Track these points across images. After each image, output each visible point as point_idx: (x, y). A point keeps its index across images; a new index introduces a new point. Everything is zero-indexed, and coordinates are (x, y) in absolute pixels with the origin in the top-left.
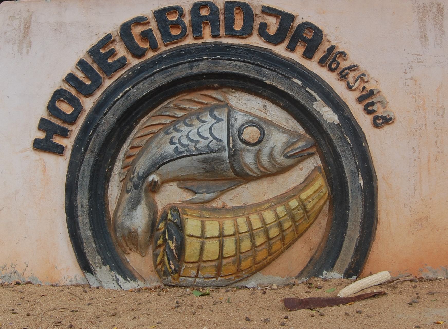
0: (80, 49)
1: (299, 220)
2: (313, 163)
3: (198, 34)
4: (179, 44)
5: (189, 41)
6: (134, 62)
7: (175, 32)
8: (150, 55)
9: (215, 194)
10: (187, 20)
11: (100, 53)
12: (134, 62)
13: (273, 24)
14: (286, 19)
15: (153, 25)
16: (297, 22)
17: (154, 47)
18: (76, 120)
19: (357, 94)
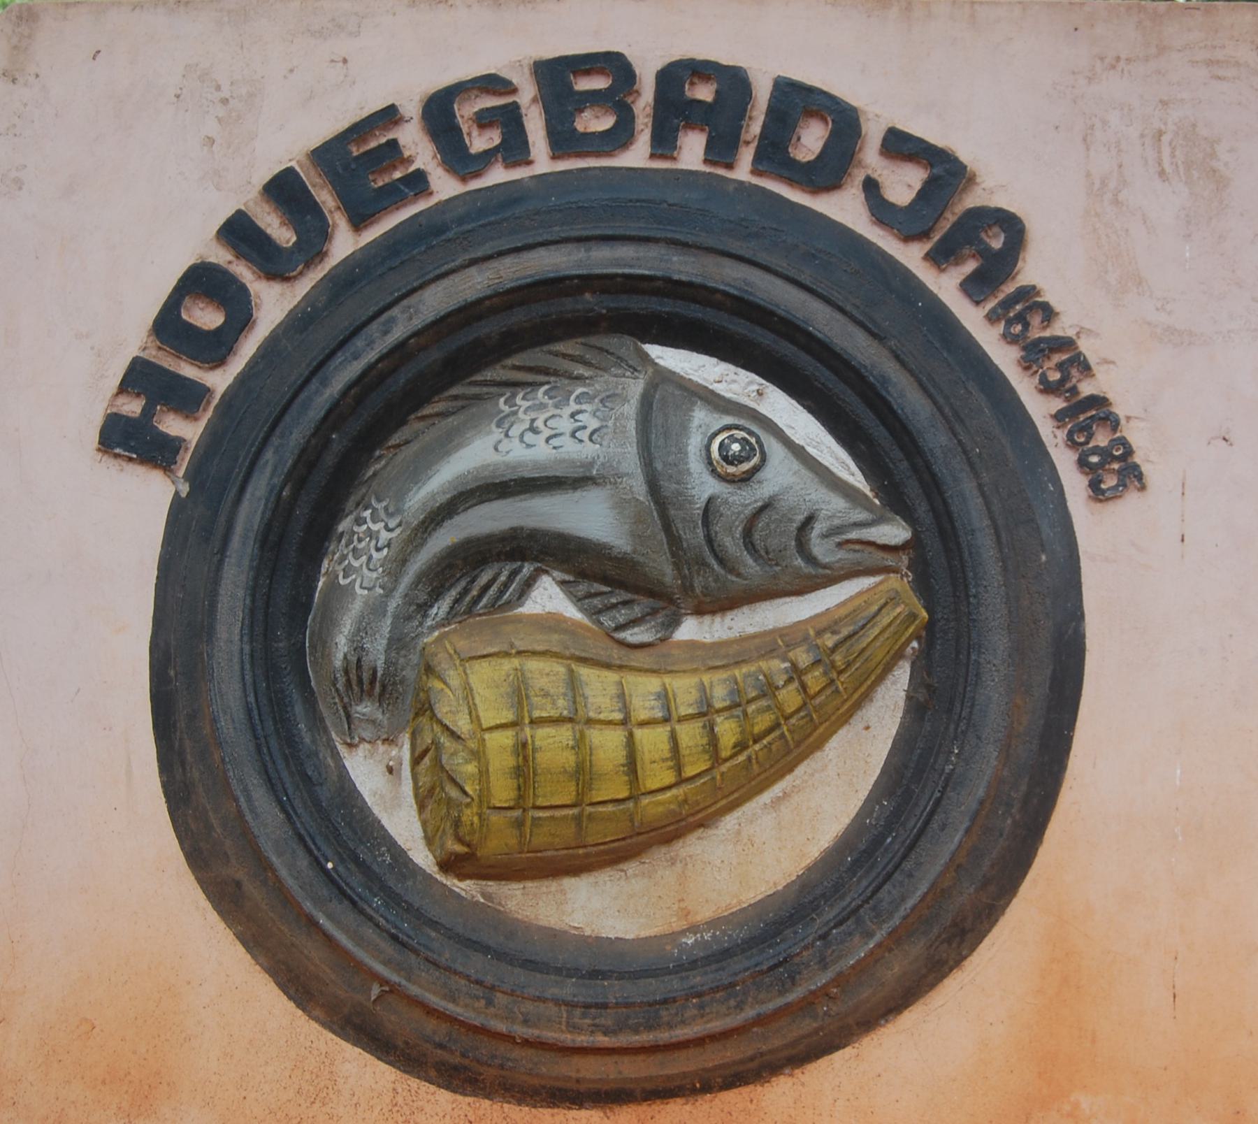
0: (290, 135)
1: (820, 692)
2: (563, 1008)
3: (664, 143)
4: (870, 494)
5: (637, 156)
6: (445, 187)
7: (596, 122)
8: (498, 175)
9: (463, 583)
10: (644, 102)
11: (358, 162)
12: (445, 187)
13: (903, 184)
14: (946, 173)
15: (527, 94)
16: (972, 200)
17: (514, 148)
18: (242, 330)
19: (1058, 404)
